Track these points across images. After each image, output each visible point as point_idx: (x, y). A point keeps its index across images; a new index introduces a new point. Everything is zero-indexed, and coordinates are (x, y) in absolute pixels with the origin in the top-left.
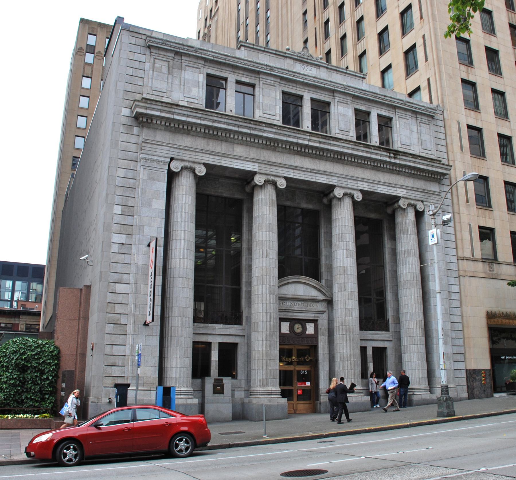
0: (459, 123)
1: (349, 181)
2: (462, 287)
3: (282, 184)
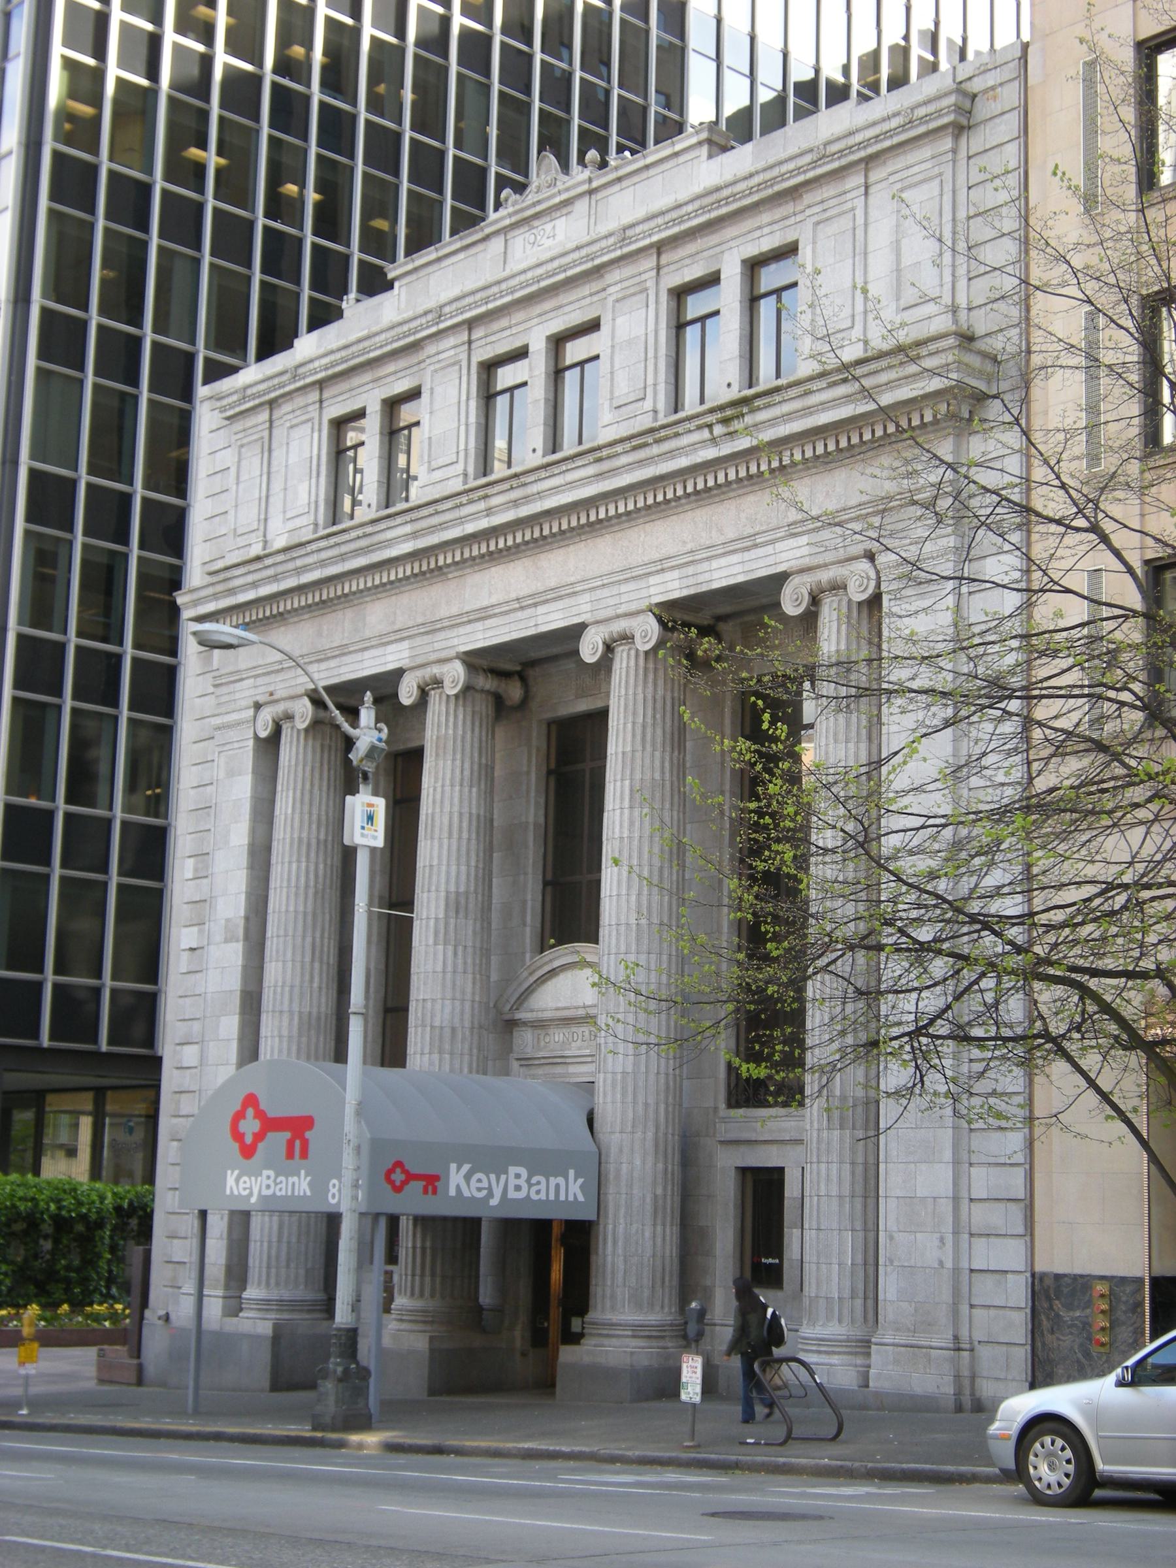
1: (624, 588)
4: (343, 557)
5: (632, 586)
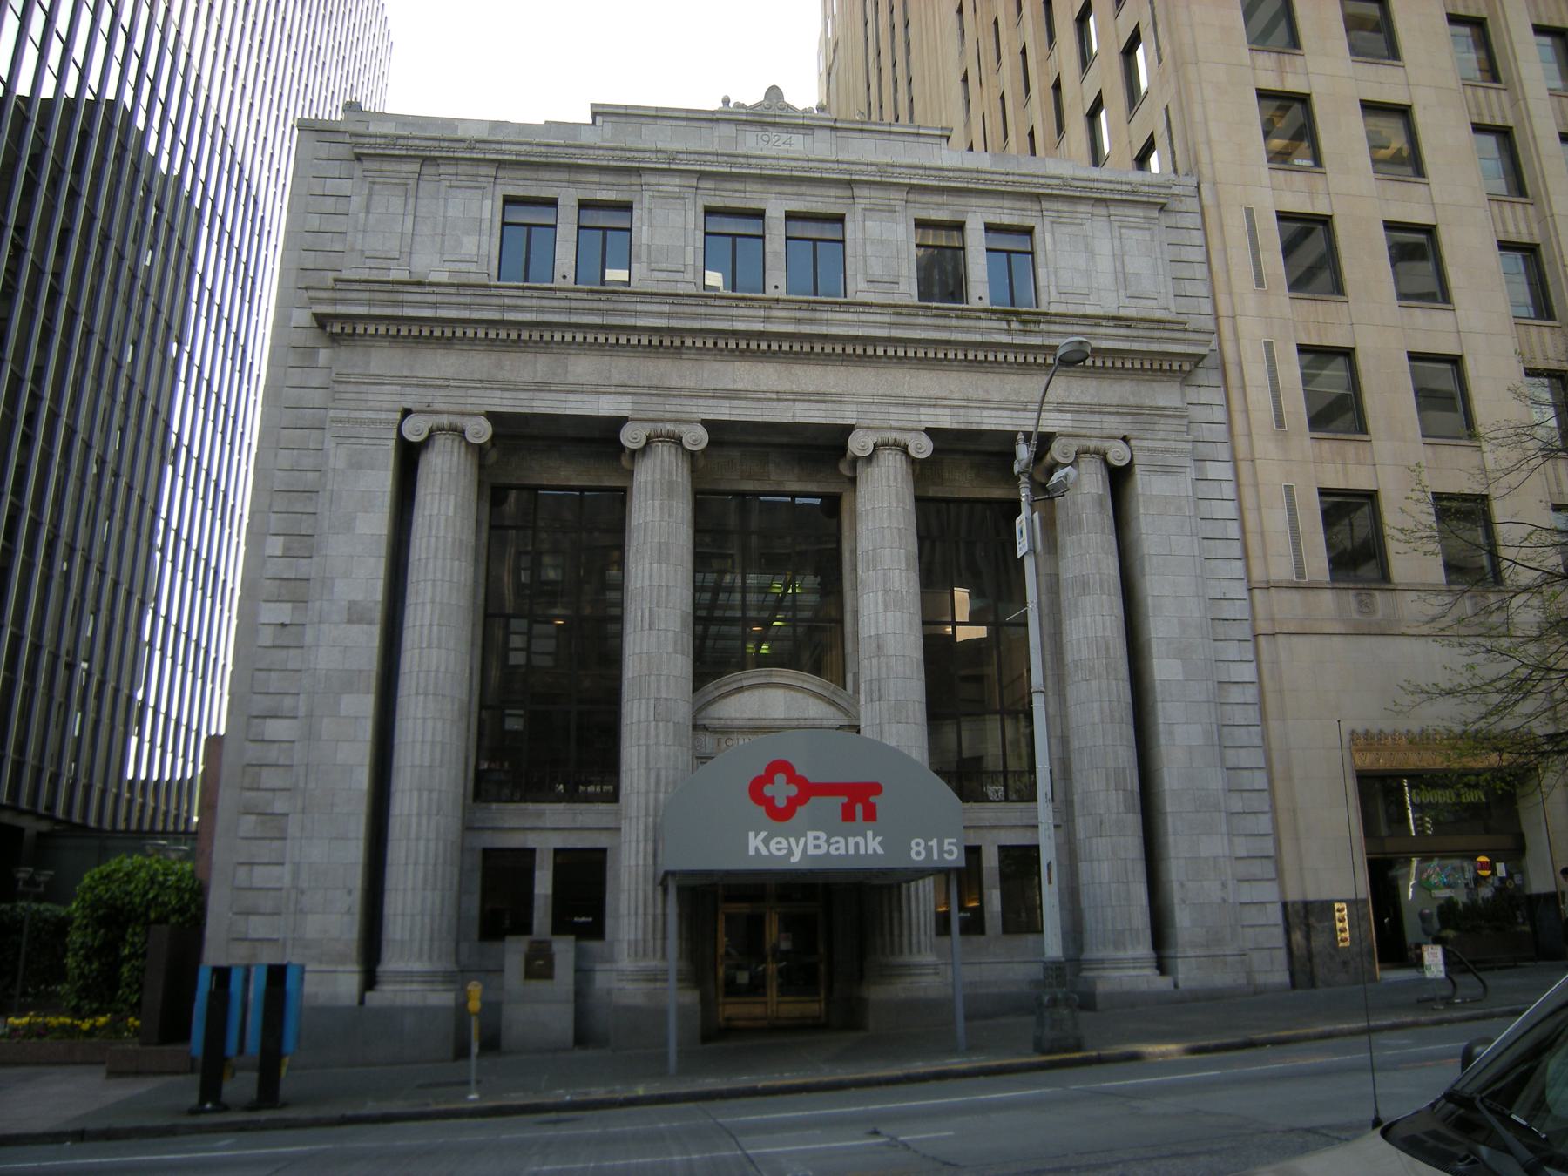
0: (1249, 212)
1: (892, 409)
2: (1265, 668)
3: (697, 438)
4: (570, 311)
5: (902, 410)
